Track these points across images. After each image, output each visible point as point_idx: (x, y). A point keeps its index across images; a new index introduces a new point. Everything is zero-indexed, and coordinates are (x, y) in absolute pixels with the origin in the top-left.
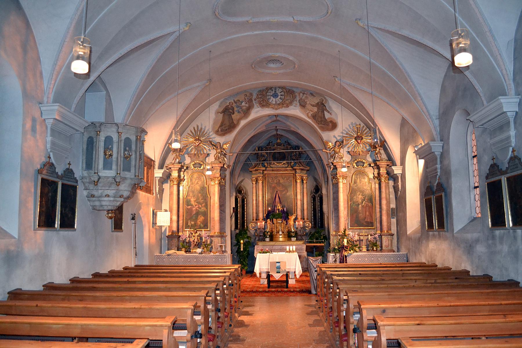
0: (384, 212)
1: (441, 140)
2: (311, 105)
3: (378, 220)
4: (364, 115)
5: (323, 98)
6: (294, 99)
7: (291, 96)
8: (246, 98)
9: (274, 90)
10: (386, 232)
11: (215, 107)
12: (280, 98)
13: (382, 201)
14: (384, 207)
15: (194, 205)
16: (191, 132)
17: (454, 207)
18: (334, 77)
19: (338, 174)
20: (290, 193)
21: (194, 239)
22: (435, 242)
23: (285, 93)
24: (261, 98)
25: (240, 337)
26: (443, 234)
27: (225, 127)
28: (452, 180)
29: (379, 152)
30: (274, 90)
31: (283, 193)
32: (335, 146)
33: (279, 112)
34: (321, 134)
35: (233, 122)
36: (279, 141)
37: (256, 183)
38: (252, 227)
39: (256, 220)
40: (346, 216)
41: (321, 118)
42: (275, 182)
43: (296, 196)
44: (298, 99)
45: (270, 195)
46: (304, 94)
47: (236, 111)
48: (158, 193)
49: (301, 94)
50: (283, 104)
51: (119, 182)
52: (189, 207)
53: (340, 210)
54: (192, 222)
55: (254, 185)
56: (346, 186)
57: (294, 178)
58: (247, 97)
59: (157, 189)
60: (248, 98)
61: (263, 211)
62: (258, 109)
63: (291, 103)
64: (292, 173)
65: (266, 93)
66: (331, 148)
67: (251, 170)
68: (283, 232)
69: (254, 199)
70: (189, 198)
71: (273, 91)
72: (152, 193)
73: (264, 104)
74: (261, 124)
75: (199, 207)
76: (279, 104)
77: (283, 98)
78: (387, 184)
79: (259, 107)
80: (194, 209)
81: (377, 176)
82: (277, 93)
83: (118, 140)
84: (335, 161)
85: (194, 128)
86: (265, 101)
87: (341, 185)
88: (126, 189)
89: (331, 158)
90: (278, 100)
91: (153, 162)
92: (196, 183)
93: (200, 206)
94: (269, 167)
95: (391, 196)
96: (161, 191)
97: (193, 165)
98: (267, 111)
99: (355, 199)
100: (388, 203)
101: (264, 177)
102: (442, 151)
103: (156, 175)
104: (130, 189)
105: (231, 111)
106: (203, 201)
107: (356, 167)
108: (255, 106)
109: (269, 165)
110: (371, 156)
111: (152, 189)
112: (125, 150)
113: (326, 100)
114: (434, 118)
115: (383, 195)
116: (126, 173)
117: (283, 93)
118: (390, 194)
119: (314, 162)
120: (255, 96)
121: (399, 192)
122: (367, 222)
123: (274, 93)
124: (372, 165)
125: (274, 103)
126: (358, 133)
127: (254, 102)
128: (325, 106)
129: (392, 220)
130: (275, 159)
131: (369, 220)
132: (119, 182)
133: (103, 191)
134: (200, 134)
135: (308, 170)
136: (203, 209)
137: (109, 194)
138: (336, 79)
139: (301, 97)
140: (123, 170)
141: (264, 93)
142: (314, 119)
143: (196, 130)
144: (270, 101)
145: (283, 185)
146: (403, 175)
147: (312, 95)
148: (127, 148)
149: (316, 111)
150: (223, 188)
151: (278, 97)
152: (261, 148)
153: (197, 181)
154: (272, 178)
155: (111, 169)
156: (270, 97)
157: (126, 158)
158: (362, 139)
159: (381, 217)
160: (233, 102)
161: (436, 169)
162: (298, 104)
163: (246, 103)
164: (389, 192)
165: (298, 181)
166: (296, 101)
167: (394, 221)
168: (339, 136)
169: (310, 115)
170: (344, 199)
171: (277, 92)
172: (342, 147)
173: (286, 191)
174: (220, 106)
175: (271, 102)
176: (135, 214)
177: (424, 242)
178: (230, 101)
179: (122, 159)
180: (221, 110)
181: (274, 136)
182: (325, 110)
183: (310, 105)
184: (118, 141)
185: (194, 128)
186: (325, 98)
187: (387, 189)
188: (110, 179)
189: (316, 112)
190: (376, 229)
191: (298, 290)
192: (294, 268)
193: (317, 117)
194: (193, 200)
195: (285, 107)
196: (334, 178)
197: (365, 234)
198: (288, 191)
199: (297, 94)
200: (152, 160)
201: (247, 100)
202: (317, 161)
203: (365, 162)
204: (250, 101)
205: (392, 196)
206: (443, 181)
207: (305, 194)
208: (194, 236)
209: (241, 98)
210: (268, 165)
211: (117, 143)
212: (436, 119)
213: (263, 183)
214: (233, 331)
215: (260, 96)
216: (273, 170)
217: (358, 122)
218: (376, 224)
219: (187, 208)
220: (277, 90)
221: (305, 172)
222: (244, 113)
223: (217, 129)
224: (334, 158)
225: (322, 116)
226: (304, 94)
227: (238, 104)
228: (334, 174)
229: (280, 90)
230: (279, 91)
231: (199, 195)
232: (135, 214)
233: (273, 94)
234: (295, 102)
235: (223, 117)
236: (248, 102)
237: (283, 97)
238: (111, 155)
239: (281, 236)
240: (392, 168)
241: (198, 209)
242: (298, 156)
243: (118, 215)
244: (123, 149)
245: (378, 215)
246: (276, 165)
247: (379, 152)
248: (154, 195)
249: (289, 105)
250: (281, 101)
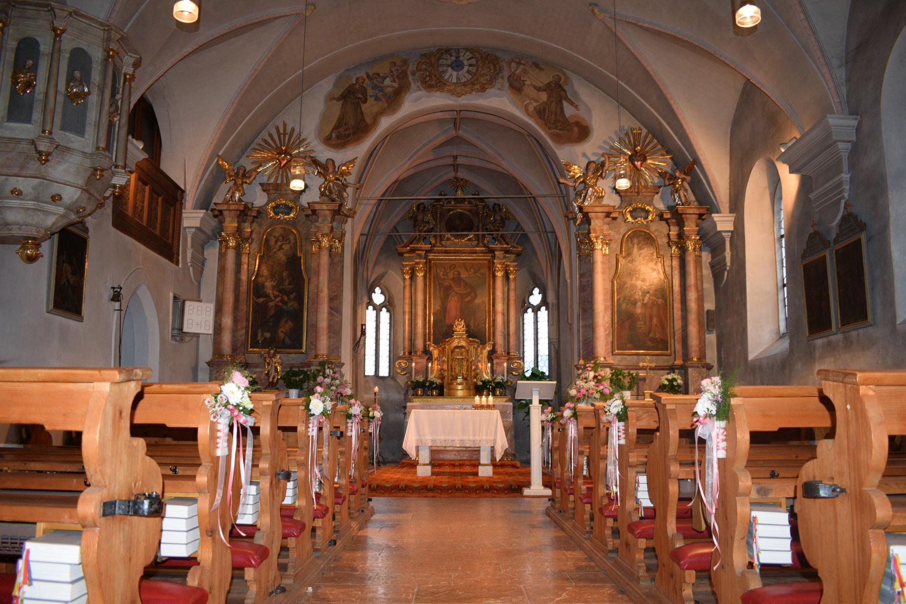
0: (692, 317)
1: (853, 112)
2: (535, 87)
3: (678, 335)
4: (651, 105)
5: (561, 75)
6: (497, 74)
7: (492, 67)
8: (393, 69)
9: (454, 54)
10: (695, 359)
11: (327, 85)
12: (468, 71)
13: (687, 293)
14: (693, 305)
15: (271, 296)
16: (271, 135)
17: (894, 263)
18: (591, 5)
19: (592, 231)
20: (481, 299)
21: (269, 372)
22: (833, 359)
23: (477, 61)
24: (426, 70)
25: (357, 571)
26: (858, 335)
27: (346, 130)
28: (890, 196)
29: (682, 185)
30: (454, 54)
31: (467, 300)
32: (585, 175)
33: (465, 102)
34: (556, 150)
35: (363, 120)
36: (460, 194)
37: (411, 278)
38: (400, 367)
39: (410, 353)
40: (607, 325)
41: (556, 115)
42: (451, 276)
43: (494, 306)
44: (506, 73)
45: (439, 303)
46: (519, 63)
47: (371, 96)
48: (189, 264)
49: (514, 65)
50: (475, 84)
51: (48, 154)
52: (261, 300)
53: (596, 311)
54: (266, 334)
55: (408, 283)
56: (609, 262)
57: (490, 270)
58: (398, 68)
59: (189, 255)
60: (398, 70)
61: (425, 335)
62: (419, 93)
63: (491, 82)
64: (486, 260)
65: (438, 60)
66: (578, 178)
67: (401, 250)
68: (465, 379)
69: (407, 309)
70: (261, 280)
71: (451, 56)
72: (175, 260)
73: (433, 83)
74: (423, 146)
75: (282, 301)
76: (465, 84)
77: (474, 71)
78: (698, 261)
79: (422, 88)
80: (271, 304)
81: (676, 240)
82: (461, 61)
83: (51, 48)
84: (586, 204)
85: (277, 129)
86: (435, 76)
87: (598, 257)
88: (70, 178)
89: (578, 197)
90: (464, 75)
91: (179, 192)
92: (277, 247)
93: (286, 299)
94: (438, 244)
95: (706, 285)
96: (200, 264)
97: (274, 208)
98: (438, 100)
99: (628, 290)
100: (700, 299)
101: (429, 267)
102: (854, 139)
103: (186, 223)
104: (81, 182)
105: (360, 96)
106: (291, 287)
107: (630, 219)
108: (413, 86)
109: (438, 241)
110: (662, 198)
111: (175, 251)
112: (70, 79)
113: (567, 78)
114: (835, 62)
115: (691, 280)
116: (72, 136)
117: (473, 61)
118: (704, 280)
119: (530, 235)
120: (412, 67)
121: (726, 273)
122: (653, 340)
123: (455, 61)
124: (665, 216)
125: (454, 81)
126: (636, 146)
127: (410, 78)
128: (564, 90)
129: (707, 336)
130: (450, 228)
131: (658, 336)
132: (48, 154)
133: (7, 179)
134: (289, 141)
135: (518, 255)
136: (292, 305)
137: (22, 189)
138: (596, 10)
139: (513, 70)
140: (63, 128)
141: (433, 61)
142: (540, 117)
143: (281, 131)
144: (446, 77)
145: (466, 284)
146: (738, 234)
147: (536, 67)
148: (77, 74)
149: (545, 100)
150: (337, 259)
151: (463, 68)
152: (422, 206)
153: (279, 243)
154: (445, 268)
155: (28, 120)
156: (445, 68)
157: (72, 97)
158: (645, 160)
159: (686, 329)
160: (365, 76)
161: (840, 184)
162: (507, 85)
163: (394, 81)
164: (702, 276)
165: (499, 274)
166: (503, 78)
167: (711, 338)
168: (594, 154)
169: (531, 108)
170: (605, 289)
171: (461, 58)
172: (601, 174)
173: (473, 294)
174: (336, 85)
175: (448, 79)
176: (121, 288)
177: (799, 366)
178: (358, 76)
179: (61, 99)
180: (338, 94)
181: (449, 181)
182: (565, 99)
183: (532, 88)
184: (51, 51)
185: (277, 129)
186: (565, 74)
187: (698, 270)
188: (23, 146)
189: (546, 103)
190: (673, 355)
191: (501, 486)
192: (493, 438)
193: (547, 114)
194: (268, 284)
195: (478, 90)
196: (582, 242)
197: (650, 365)
198: (476, 296)
199: (504, 64)
200: (177, 187)
201: (395, 73)
202: (536, 235)
203: (651, 210)
204: (403, 76)
205: (709, 285)
206: (862, 210)
207: (512, 303)
208: (269, 364)
209: (383, 68)
210: (436, 241)
211: (50, 57)
212: (840, 67)
213: (425, 276)
214: (341, 558)
215: (424, 67)
216: (446, 252)
217: (636, 124)
218: (673, 346)
219: (255, 302)
220: (461, 54)
221: (513, 257)
222: (387, 102)
223: (327, 134)
224: (585, 196)
225: (559, 111)
226: (519, 63)
227: (375, 81)
228: (582, 234)
229: (468, 55)
230: (464, 58)
231: (284, 275)
232: (121, 288)
233: (452, 63)
234: (499, 81)
235: (342, 108)
236: (397, 77)
237: (474, 70)
238: (29, 84)
239: (460, 387)
240: (713, 217)
241: (280, 304)
242: (500, 223)
243: (70, 276)
244: (65, 75)
245: (678, 325)
246: (452, 241)
247: (682, 185)
248: (180, 265)
249: (486, 86)
250: (470, 77)
